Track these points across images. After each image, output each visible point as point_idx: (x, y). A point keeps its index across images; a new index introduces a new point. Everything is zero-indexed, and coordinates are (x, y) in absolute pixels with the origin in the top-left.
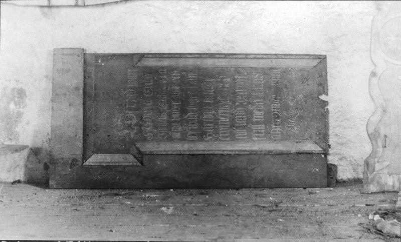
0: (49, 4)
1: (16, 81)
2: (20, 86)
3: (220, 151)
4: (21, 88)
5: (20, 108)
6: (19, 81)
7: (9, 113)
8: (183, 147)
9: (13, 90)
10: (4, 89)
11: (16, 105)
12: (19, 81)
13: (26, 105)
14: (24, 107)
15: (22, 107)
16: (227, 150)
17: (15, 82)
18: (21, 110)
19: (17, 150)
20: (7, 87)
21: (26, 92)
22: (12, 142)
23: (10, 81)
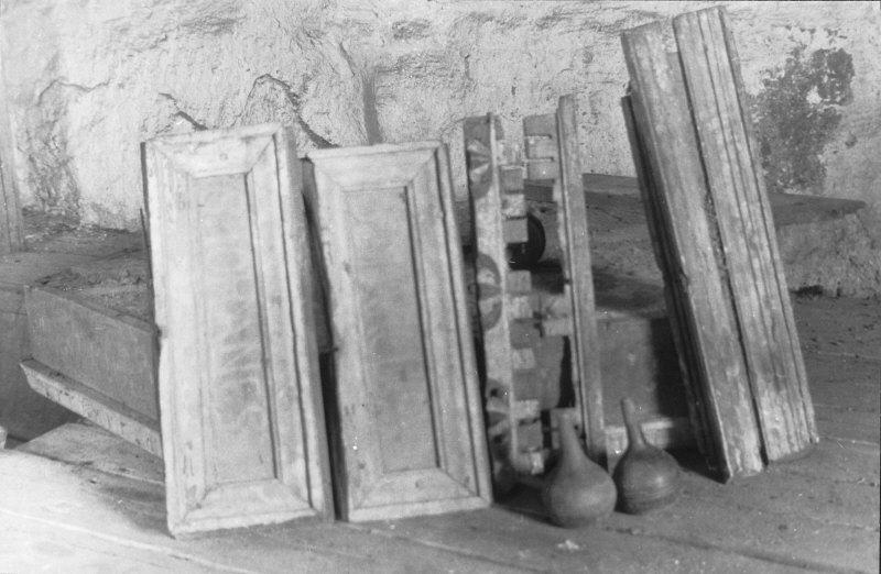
0: (540, 297)
1: (830, 33)
2: (839, 44)
3: (419, 234)
4: (841, 50)
5: (833, 102)
6: (836, 32)
7: (805, 115)
8: (760, 368)
9: (820, 53)
10: (796, 52)
11: (822, 93)
12: (836, 32)
13: (850, 96)
14: (843, 100)
15: (838, 99)
16: (419, 234)
17: (826, 33)
18: (837, 107)
19: (834, 211)
20: (805, 47)
21: (853, 62)
22: (804, 188)
23: (813, 31)
